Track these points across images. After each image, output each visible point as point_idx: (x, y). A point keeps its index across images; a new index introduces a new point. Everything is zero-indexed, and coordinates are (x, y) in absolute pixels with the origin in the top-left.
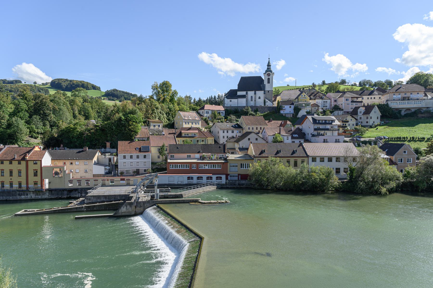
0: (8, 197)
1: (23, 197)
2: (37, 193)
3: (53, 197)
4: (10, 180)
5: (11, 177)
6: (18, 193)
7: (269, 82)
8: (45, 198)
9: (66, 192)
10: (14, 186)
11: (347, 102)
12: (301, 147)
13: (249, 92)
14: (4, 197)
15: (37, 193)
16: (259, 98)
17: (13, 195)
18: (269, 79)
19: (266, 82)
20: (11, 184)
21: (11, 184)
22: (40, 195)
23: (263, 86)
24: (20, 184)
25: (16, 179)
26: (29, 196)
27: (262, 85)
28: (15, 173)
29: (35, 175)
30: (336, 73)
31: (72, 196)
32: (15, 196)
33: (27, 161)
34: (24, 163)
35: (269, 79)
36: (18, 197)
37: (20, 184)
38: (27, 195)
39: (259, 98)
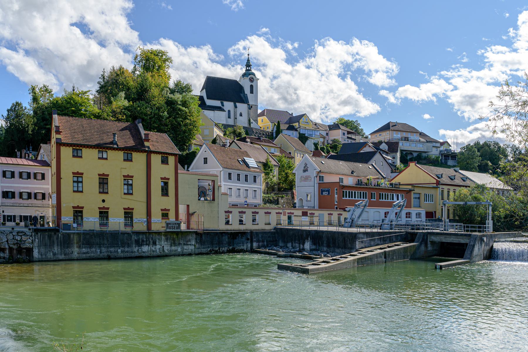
0: (112, 249)
1: (145, 248)
2: (174, 240)
3: (204, 250)
4: (102, 205)
5: (104, 196)
6: (134, 237)
7: (252, 92)
8: (135, 255)
9: (226, 239)
10: (111, 220)
11: (344, 137)
12: (191, 211)
13: (225, 103)
14: (104, 250)
15: (174, 240)
16: (241, 115)
17: (123, 245)
18: (252, 86)
19: (247, 91)
20: (104, 214)
21: (104, 214)
22: (179, 244)
23: (244, 96)
24: (128, 214)
25: (117, 203)
26: (158, 247)
27: (242, 95)
28: (116, 185)
29: (165, 191)
30: (438, 73)
31: (238, 248)
32: (129, 246)
33: (149, 153)
34: (139, 158)
35: (252, 86)
36: (136, 249)
37: (128, 214)
38: (155, 243)
39: (241, 115)
